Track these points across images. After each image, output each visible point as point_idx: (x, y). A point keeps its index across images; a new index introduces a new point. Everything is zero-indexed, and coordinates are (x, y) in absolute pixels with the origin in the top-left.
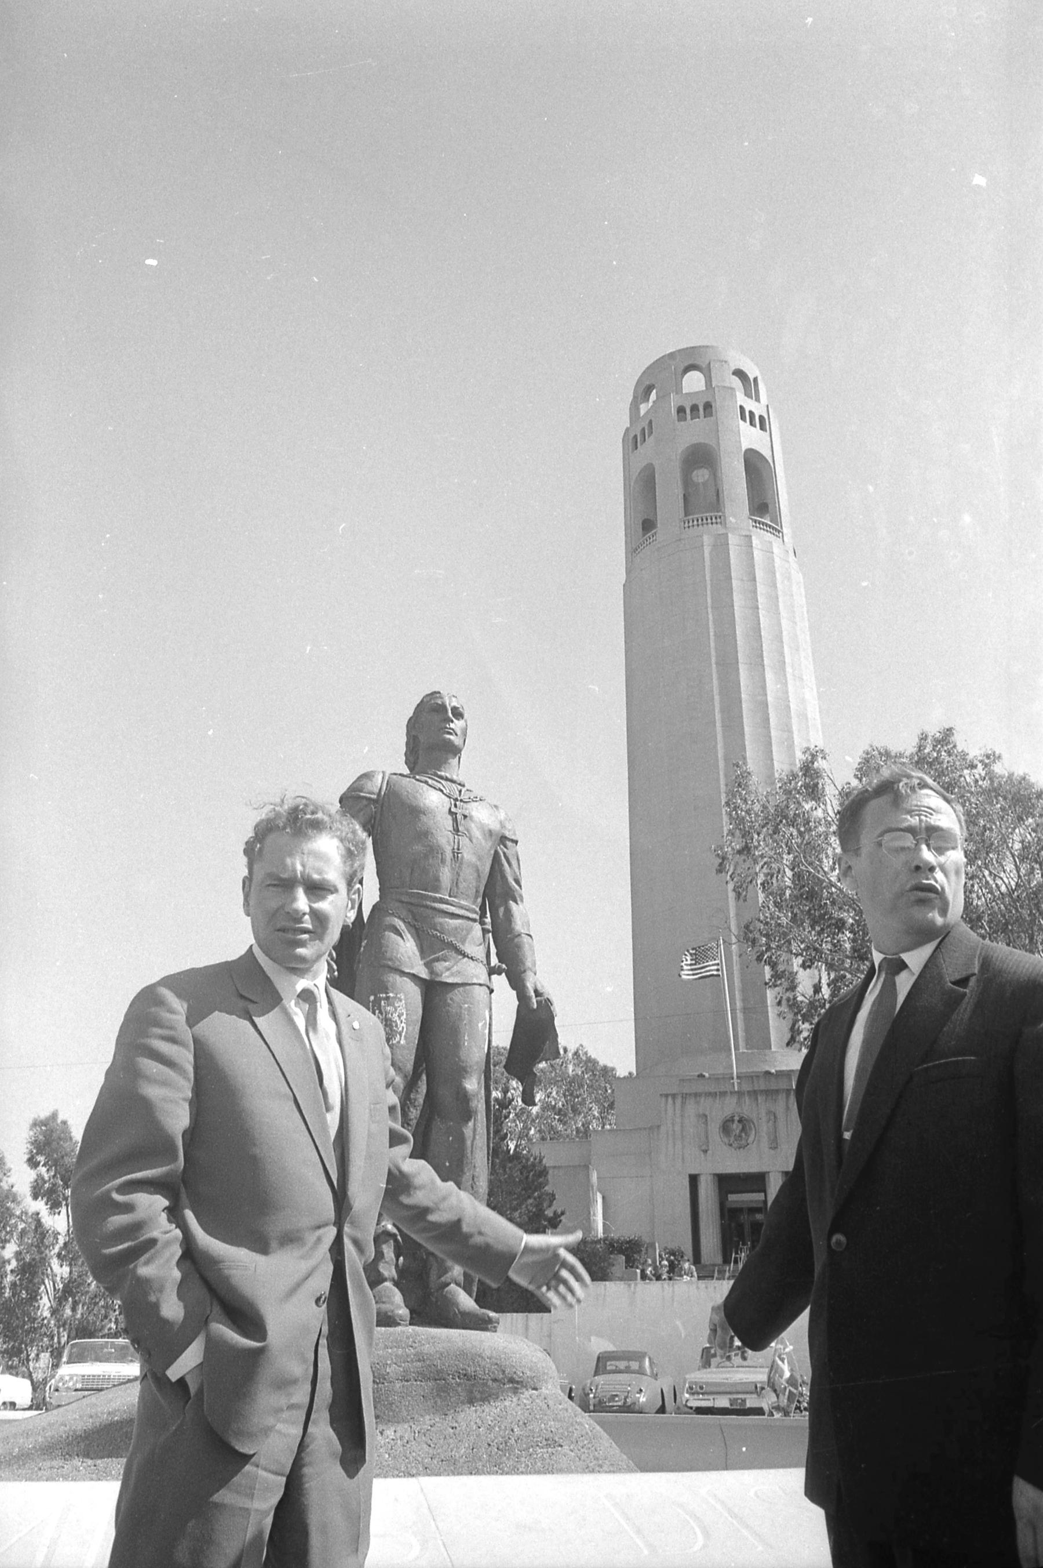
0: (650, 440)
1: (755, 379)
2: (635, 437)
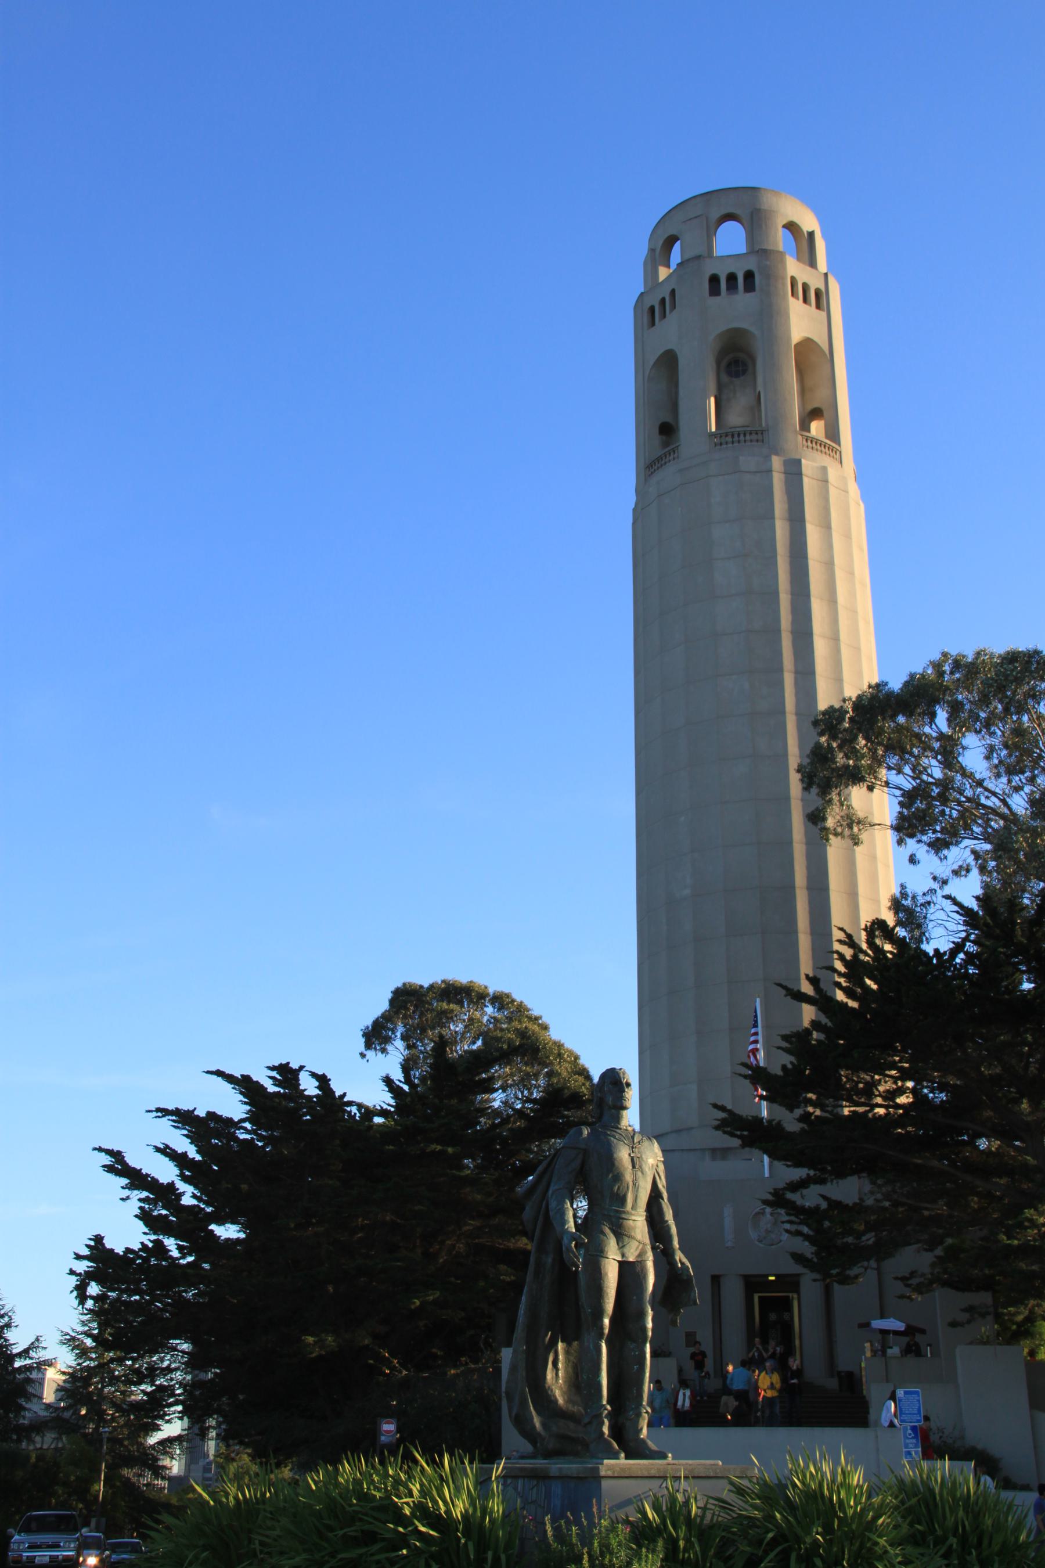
0: (672, 317)
1: (811, 235)
2: (652, 309)
